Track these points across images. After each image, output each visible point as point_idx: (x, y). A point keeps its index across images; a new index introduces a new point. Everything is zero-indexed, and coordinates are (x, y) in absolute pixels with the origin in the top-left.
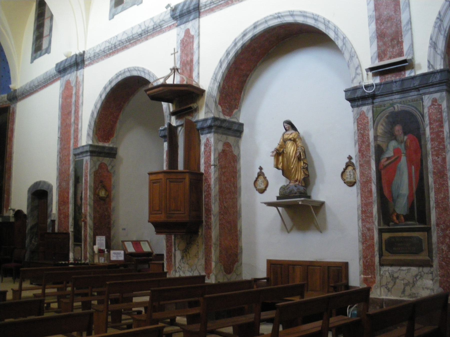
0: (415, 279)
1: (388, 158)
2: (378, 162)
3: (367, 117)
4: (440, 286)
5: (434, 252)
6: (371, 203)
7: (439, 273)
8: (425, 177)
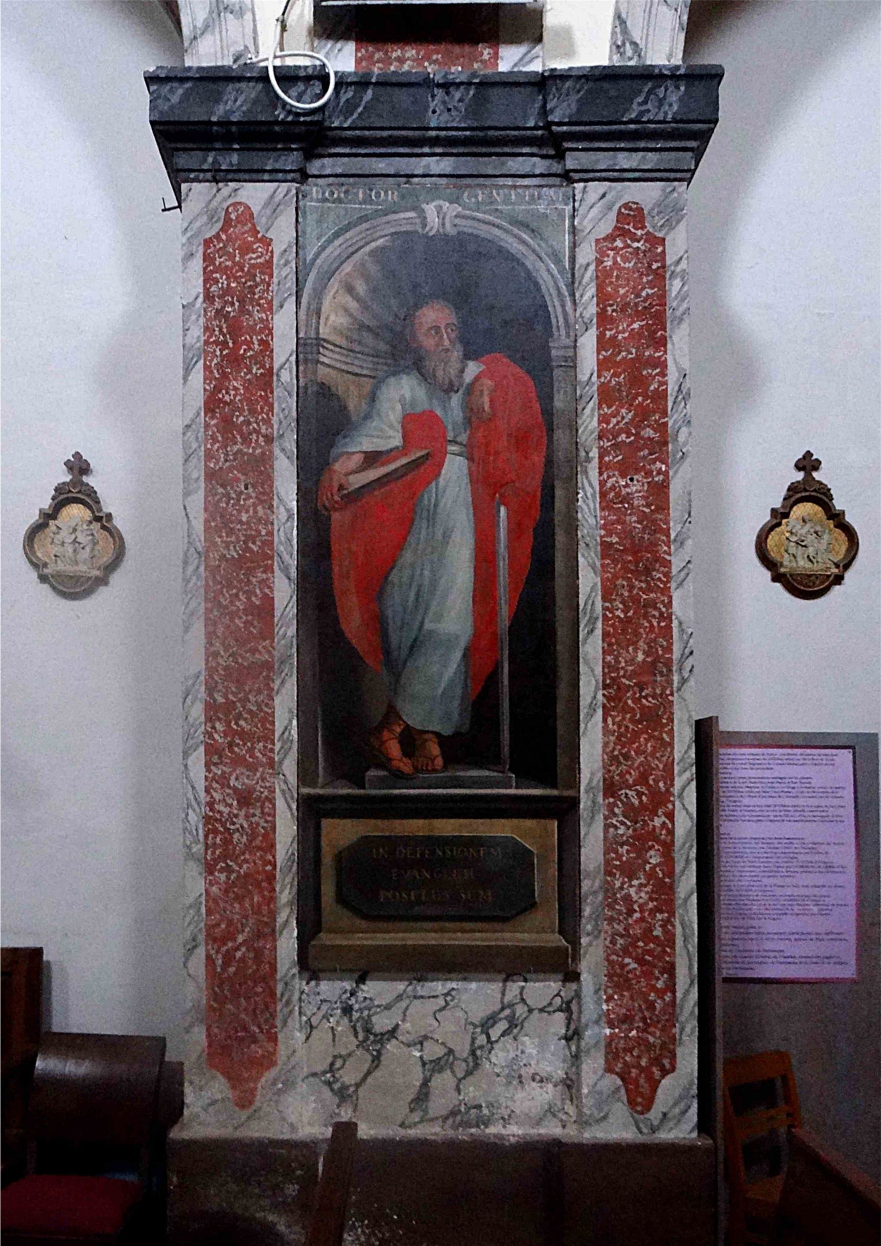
0: (482, 1040)
1: (372, 458)
2: (313, 468)
3: (267, 242)
4: (609, 1070)
5: (587, 911)
6: (268, 666)
7: (605, 1007)
8: (559, 565)
